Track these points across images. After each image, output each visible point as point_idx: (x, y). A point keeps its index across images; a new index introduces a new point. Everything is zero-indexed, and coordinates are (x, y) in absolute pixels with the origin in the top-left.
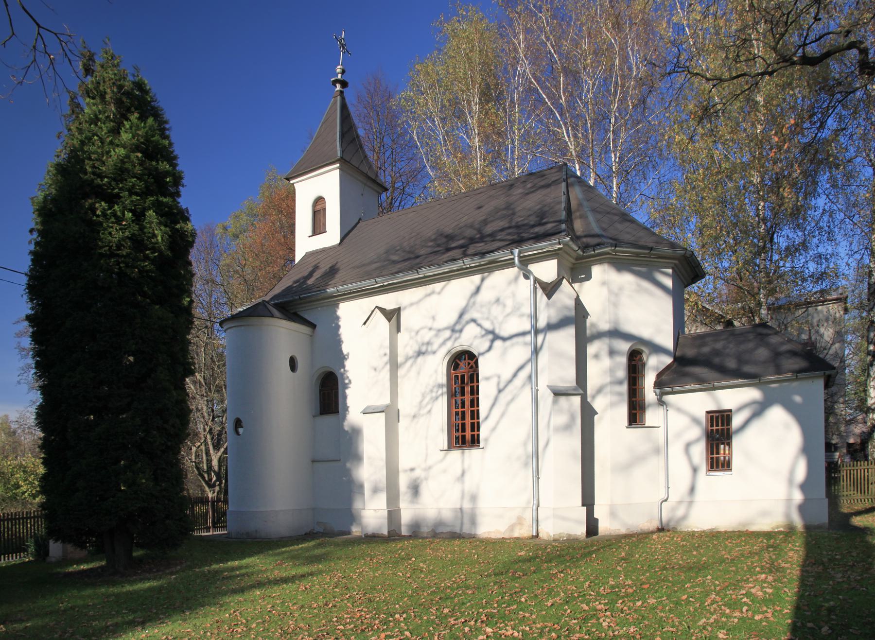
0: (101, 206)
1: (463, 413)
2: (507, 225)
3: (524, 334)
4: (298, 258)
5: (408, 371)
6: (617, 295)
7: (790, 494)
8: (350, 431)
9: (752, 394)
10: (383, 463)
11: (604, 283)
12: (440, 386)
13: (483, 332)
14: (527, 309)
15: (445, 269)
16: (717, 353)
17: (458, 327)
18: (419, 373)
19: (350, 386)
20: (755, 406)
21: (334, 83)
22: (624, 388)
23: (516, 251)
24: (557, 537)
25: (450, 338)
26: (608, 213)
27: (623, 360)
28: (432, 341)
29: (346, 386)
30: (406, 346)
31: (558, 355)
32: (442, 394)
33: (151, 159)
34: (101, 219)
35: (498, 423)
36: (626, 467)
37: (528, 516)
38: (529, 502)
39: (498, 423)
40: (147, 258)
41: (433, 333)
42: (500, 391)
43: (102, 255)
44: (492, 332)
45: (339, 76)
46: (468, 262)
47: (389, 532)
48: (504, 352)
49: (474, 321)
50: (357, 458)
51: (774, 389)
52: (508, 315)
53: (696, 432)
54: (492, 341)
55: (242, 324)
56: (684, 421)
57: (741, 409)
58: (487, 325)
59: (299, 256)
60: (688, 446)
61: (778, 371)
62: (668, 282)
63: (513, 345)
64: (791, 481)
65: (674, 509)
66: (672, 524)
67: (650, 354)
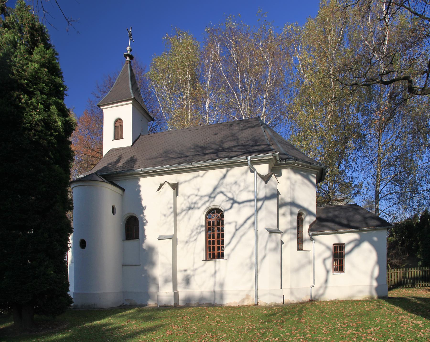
0: (24, 98)
1: (213, 241)
2: (236, 144)
3: (250, 201)
4: (105, 152)
5: (183, 217)
6: (294, 185)
7: (371, 282)
8: (147, 249)
9: (354, 236)
10: (171, 267)
11: (289, 178)
12: (202, 226)
13: (227, 199)
14: (252, 188)
15: (207, 164)
16: (336, 216)
17: (213, 195)
18: (189, 219)
19: (147, 224)
20: (356, 242)
21: (126, 56)
22: (296, 231)
23: (249, 158)
24: (270, 304)
25: (208, 201)
26: (285, 144)
27: (296, 217)
28: (198, 202)
29: (144, 224)
30: (181, 204)
31: (270, 212)
32: (203, 231)
33: (52, 74)
34: (25, 106)
35: (235, 246)
36: (297, 270)
37: (252, 294)
38: (252, 287)
39: (235, 246)
40: (51, 135)
41: (198, 198)
42: (237, 230)
43: (25, 129)
44: (233, 199)
45: (129, 52)
46: (222, 161)
47: (174, 304)
48: (239, 210)
49: (222, 192)
50: (153, 264)
51: (365, 234)
52: (241, 191)
53: (328, 254)
54: (232, 204)
55: (85, 184)
56: (323, 248)
57: (350, 243)
58: (230, 195)
59: (105, 151)
60: (324, 260)
61: (367, 225)
62: (315, 181)
63: (244, 206)
64: (372, 276)
65: (318, 290)
66: (317, 297)
67: (307, 215)
